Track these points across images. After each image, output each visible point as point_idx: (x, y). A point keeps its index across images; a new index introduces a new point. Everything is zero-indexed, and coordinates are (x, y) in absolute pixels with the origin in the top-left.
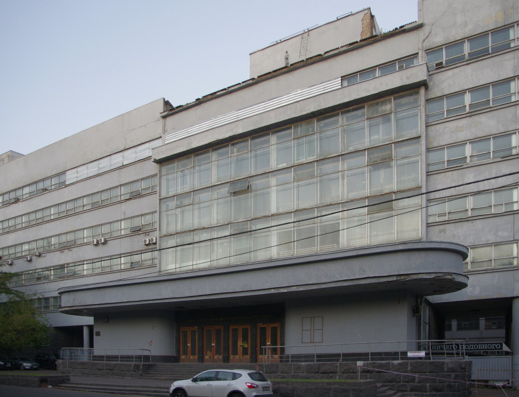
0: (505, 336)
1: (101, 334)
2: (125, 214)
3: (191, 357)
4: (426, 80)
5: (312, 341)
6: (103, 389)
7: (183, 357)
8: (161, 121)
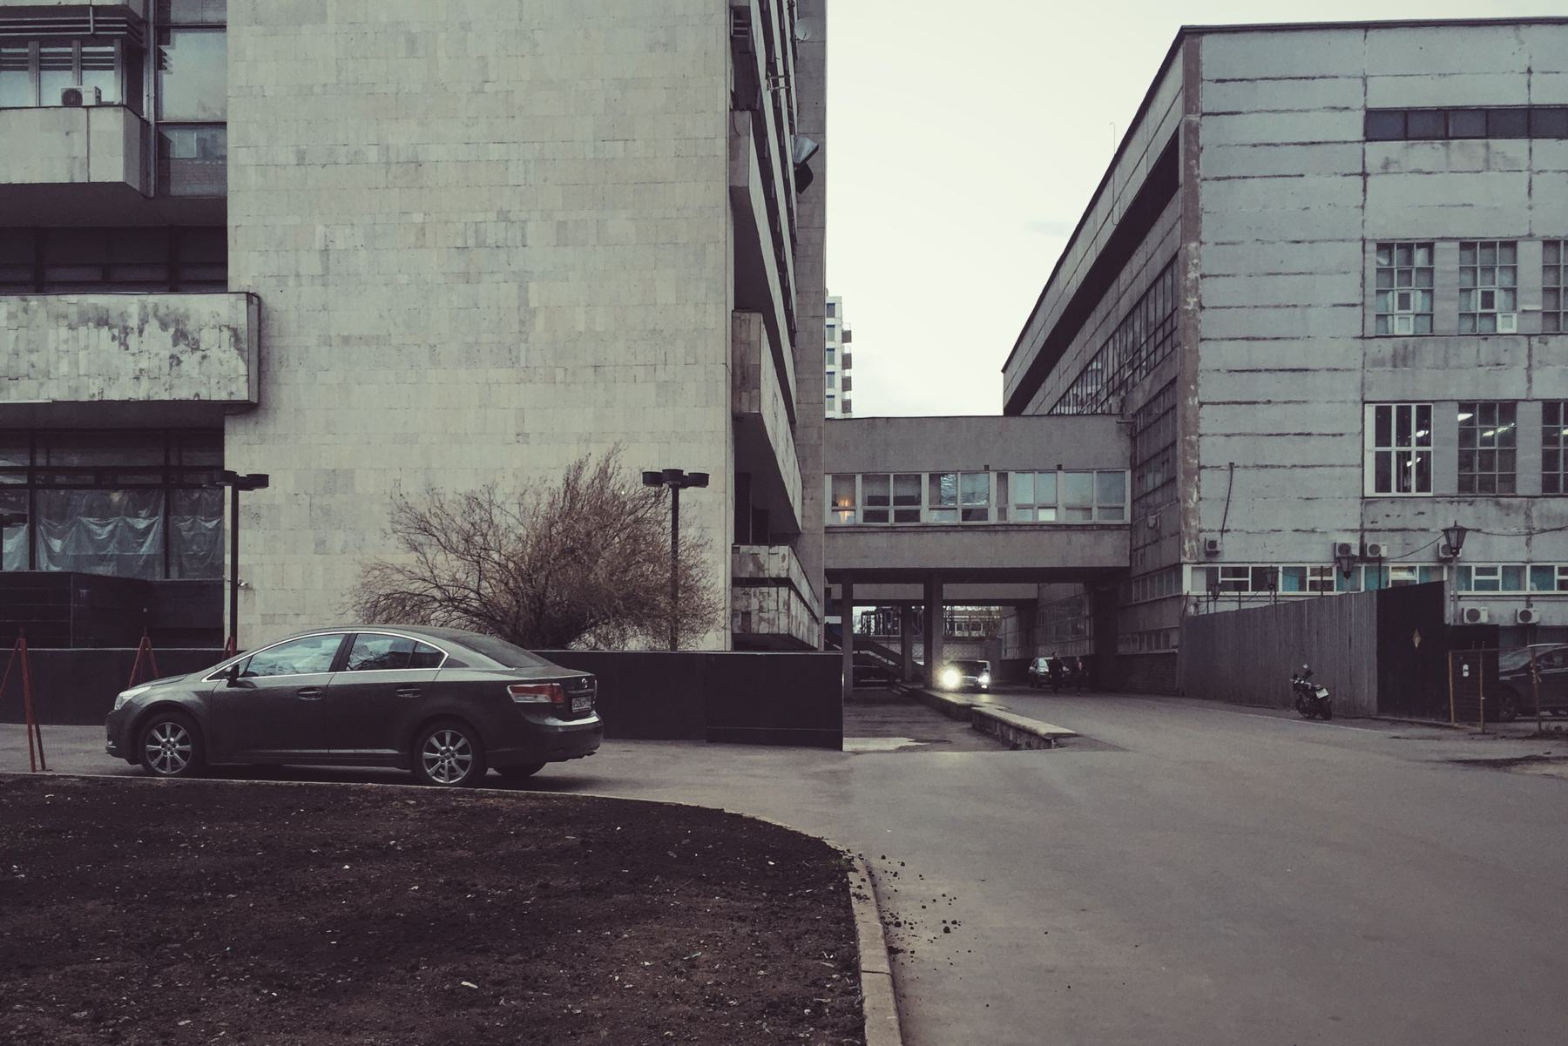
0: (91, 181)
6: (56, 61)
8: (1361, 74)
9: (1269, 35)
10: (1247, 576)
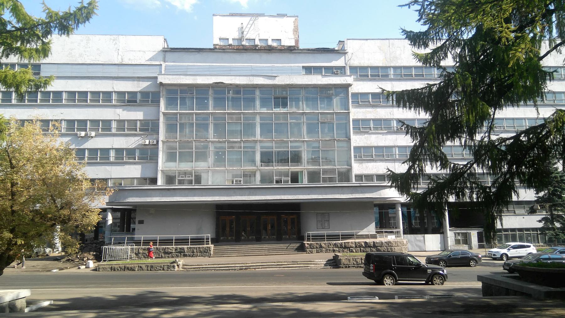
1: (145, 222)
2: (119, 116)
3: (229, 238)
4: (232, 174)
5: (323, 227)
6: (267, 265)
7: (222, 238)
9: (160, 191)
10: (215, 108)
